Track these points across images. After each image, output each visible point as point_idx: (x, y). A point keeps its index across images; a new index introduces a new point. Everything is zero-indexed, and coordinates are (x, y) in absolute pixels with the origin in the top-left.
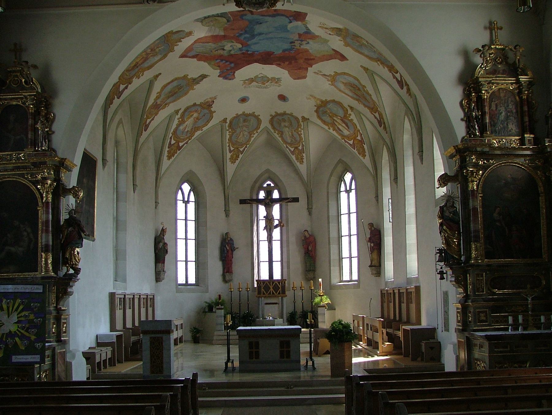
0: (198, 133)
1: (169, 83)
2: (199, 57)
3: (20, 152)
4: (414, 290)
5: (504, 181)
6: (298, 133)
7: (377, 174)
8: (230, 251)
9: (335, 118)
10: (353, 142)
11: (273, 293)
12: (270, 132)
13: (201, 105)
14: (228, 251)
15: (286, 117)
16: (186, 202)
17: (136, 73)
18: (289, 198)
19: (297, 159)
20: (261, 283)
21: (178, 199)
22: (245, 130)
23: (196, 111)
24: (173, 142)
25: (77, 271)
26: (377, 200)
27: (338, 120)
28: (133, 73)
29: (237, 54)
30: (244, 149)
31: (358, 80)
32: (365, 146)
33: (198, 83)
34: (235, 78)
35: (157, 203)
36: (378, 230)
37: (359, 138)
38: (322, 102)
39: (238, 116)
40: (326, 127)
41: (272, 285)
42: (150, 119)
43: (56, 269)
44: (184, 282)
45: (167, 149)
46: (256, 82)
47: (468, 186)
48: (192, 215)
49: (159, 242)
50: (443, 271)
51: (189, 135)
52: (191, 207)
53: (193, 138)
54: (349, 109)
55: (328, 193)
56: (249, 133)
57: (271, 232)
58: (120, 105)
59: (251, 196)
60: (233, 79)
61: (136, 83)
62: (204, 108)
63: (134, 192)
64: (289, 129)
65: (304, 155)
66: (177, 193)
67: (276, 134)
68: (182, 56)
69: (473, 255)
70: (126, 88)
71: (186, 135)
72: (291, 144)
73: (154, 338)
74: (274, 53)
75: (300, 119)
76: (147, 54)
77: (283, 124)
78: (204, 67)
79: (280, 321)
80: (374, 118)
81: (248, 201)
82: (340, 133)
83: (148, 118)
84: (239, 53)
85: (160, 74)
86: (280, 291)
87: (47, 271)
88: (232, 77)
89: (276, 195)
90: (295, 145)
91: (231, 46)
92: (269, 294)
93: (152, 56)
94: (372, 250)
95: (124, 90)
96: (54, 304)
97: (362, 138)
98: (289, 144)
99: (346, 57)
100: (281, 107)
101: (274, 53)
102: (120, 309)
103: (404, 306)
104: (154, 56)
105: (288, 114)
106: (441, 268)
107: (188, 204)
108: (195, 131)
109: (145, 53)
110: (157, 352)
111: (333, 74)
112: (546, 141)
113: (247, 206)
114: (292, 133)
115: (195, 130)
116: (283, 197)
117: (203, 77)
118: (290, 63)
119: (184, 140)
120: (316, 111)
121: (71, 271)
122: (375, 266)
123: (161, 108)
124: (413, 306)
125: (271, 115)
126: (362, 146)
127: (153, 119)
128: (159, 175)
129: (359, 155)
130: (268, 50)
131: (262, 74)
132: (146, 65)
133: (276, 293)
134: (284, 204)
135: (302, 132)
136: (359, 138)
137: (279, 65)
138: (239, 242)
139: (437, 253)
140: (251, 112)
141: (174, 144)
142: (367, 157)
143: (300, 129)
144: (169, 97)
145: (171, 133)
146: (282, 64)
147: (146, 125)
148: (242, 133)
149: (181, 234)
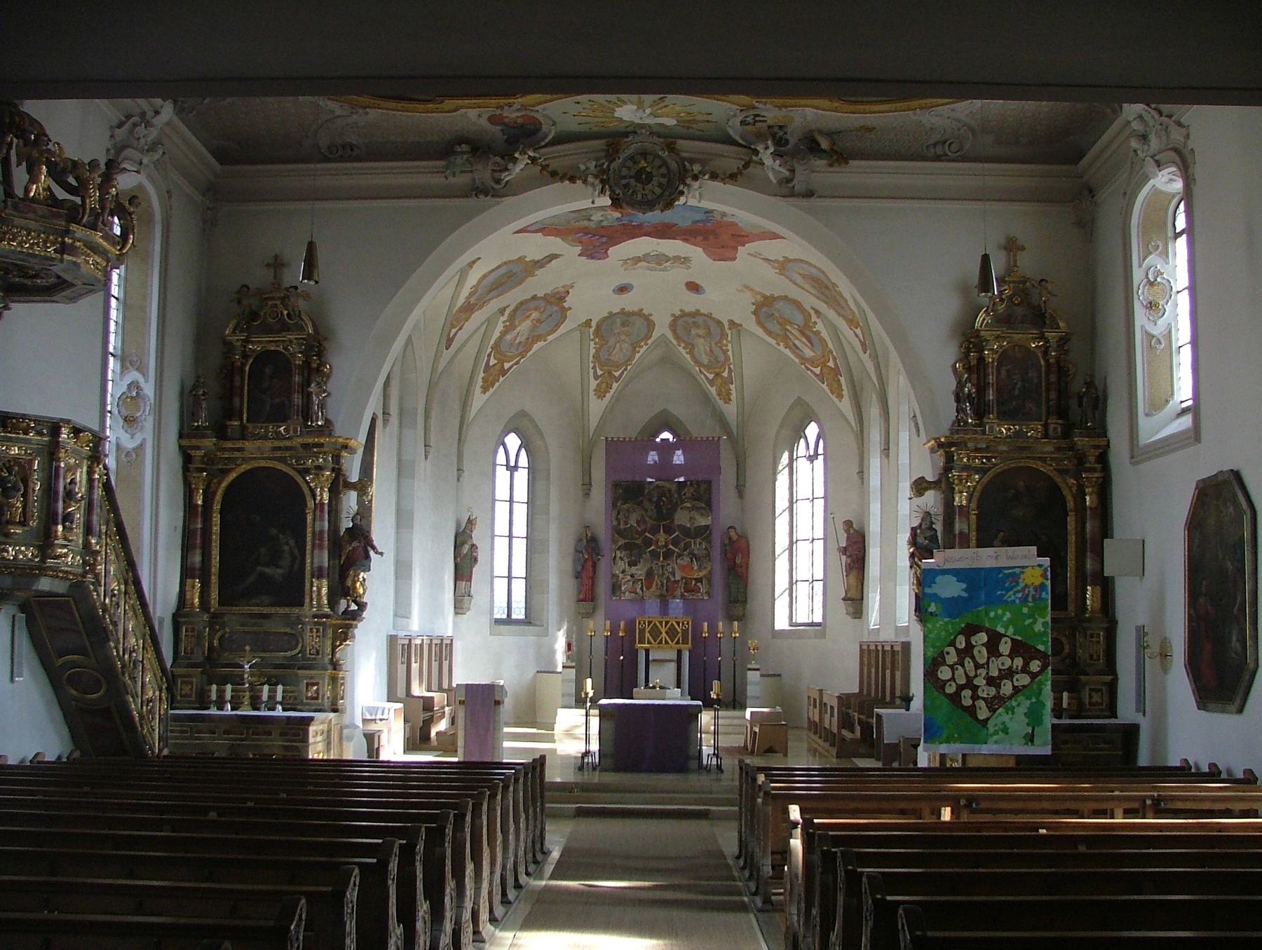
1: (493, 270)
3: (280, 424)
5: (1013, 491)
6: (721, 348)
7: (862, 431)
9: (788, 327)
11: (667, 642)
13: (545, 298)
15: (699, 320)
16: (513, 469)
20: (644, 623)
21: (497, 463)
22: (624, 340)
23: (536, 309)
24: (493, 362)
25: (362, 606)
26: (862, 479)
27: (793, 331)
30: (623, 373)
31: (823, 273)
32: (842, 379)
37: (831, 364)
38: (765, 297)
39: (611, 315)
40: (773, 342)
41: (666, 626)
43: (333, 603)
44: (505, 616)
45: (482, 375)
48: (521, 493)
49: (463, 543)
52: (522, 477)
54: (812, 312)
56: (632, 344)
60: (605, 258)
62: (551, 303)
63: (426, 458)
65: (732, 387)
66: (495, 452)
67: (681, 349)
71: (517, 350)
72: (708, 367)
75: (726, 326)
78: (555, 244)
82: (797, 353)
83: (453, 326)
85: (479, 258)
86: (679, 639)
87: (320, 605)
90: (715, 368)
94: (849, 569)
96: (329, 655)
97: (836, 365)
98: (704, 366)
100: (691, 302)
102: (402, 663)
103: (888, 672)
105: (705, 315)
107: (515, 473)
114: (710, 347)
115: (533, 341)
117: (553, 257)
121: (354, 607)
122: (852, 600)
125: (673, 315)
127: (460, 329)
128: (466, 420)
136: (831, 364)
137: (686, 240)
140: (636, 309)
142: (846, 400)
143: (725, 342)
148: (618, 345)
149: (501, 527)
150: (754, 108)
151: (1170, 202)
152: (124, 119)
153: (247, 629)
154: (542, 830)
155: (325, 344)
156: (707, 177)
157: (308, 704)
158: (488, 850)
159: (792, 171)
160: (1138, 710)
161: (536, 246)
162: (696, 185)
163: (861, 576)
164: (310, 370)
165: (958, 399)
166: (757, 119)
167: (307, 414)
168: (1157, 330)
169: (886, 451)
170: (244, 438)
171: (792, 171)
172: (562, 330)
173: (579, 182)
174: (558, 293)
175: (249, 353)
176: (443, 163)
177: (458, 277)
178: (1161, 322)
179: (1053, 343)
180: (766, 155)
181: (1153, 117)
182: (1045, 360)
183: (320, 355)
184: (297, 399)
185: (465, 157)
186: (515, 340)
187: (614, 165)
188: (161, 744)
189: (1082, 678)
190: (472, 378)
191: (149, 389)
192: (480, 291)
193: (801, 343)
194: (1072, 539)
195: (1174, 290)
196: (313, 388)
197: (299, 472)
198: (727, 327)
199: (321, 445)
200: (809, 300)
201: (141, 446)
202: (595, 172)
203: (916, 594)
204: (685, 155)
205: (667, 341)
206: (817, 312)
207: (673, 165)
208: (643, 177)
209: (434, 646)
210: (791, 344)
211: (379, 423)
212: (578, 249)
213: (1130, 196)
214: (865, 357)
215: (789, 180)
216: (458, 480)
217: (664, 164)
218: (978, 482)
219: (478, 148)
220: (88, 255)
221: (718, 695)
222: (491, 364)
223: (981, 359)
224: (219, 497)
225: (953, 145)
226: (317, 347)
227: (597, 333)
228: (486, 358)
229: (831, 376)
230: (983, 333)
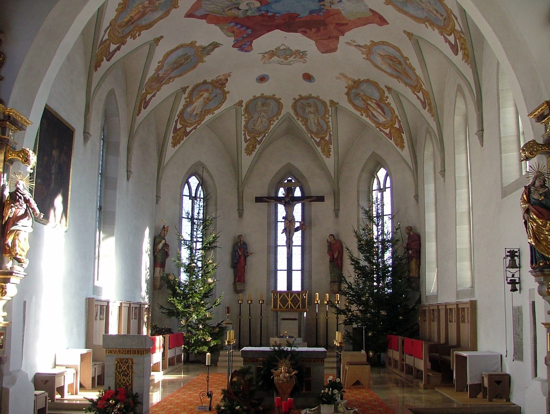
0: (208, 117)
1: (173, 51)
4: (468, 306)
6: (324, 120)
8: (243, 257)
9: (369, 102)
10: (390, 130)
12: (293, 120)
14: (240, 256)
15: (310, 101)
17: (130, 32)
18: (313, 196)
19: (323, 152)
22: (262, 116)
23: (207, 90)
24: (179, 126)
26: (417, 200)
27: (372, 105)
28: (127, 30)
29: (255, 16)
30: (262, 139)
31: (399, 51)
32: (404, 136)
33: (208, 54)
34: (253, 50)
35: (158, 197)
36: (418, 235)
37: (397, 126)
38: (355, 82)
39: (255, 99)
40: (358, 113)
41: (291, 297)
42: (151, 95)
45: (172, 135)
46: (278, 57)
50: (516, 280)
51: (199, 119)
53: (203, 122)
54: (385, 89)
55: (358, 191)
57: (291, 235)
58: (109, 70)
61: (131, 44)
64: (314, 115)
65: (332, 146)
67: (299, 122)
68: (189, 15)
70: (118, 48)
72: (316, 134)
74: (300, 15)
76: (144, 7)
77: (308, 110)
79: (299, 340)
80: (417, 99)
81: (265, 198)
83: (147, 93)
84: (257, 14)
85: (162, 37)
89: (298, 193)
91: (247, 4)
92: (286, 308)
93: (151, 11)
95: (115, 51)
99: (387, 20)
100: (306, 89)
101: (300, 15)
104: (153, 11)
106: (513, 276)
108: (205, 115)
109: (142, 5)
110: (124, 380)
111: (369, 44)
113: (264, 205)
116: (306, 195)
117: (215, 45)
119: (191, 124)
120: (347, 94)
123: (163, 82)
125: (294, 99)
126: (400, 136)
127: (154, 96)
129: (396, 147)
130: (292, 11)
131: (284, 45)
132: (143, 22)
133: (295, 306)
134: (306, 202)
135: (330, 119)
136: (397, 126)
137: (304, 33)
139: (507, 256)
140: (271, 95)
141: (180, 128)
143: (327, 116)
144: (173, 69)
145: (176, 116)
146: (308, 31)
147: (145, 102)
148: (259, 119)
163: (418, 263)
172: (224, 107)
174: (220, 80)
186: (193, 112)
192: (165, 67)
198: (328, 105)
203: (531, 246)
205: (291, 117)
210: (371, 114)
216: (157, 203)
221: (340, 343)
222: (178, 128)
227: (246, 111)
228: (174, 124)
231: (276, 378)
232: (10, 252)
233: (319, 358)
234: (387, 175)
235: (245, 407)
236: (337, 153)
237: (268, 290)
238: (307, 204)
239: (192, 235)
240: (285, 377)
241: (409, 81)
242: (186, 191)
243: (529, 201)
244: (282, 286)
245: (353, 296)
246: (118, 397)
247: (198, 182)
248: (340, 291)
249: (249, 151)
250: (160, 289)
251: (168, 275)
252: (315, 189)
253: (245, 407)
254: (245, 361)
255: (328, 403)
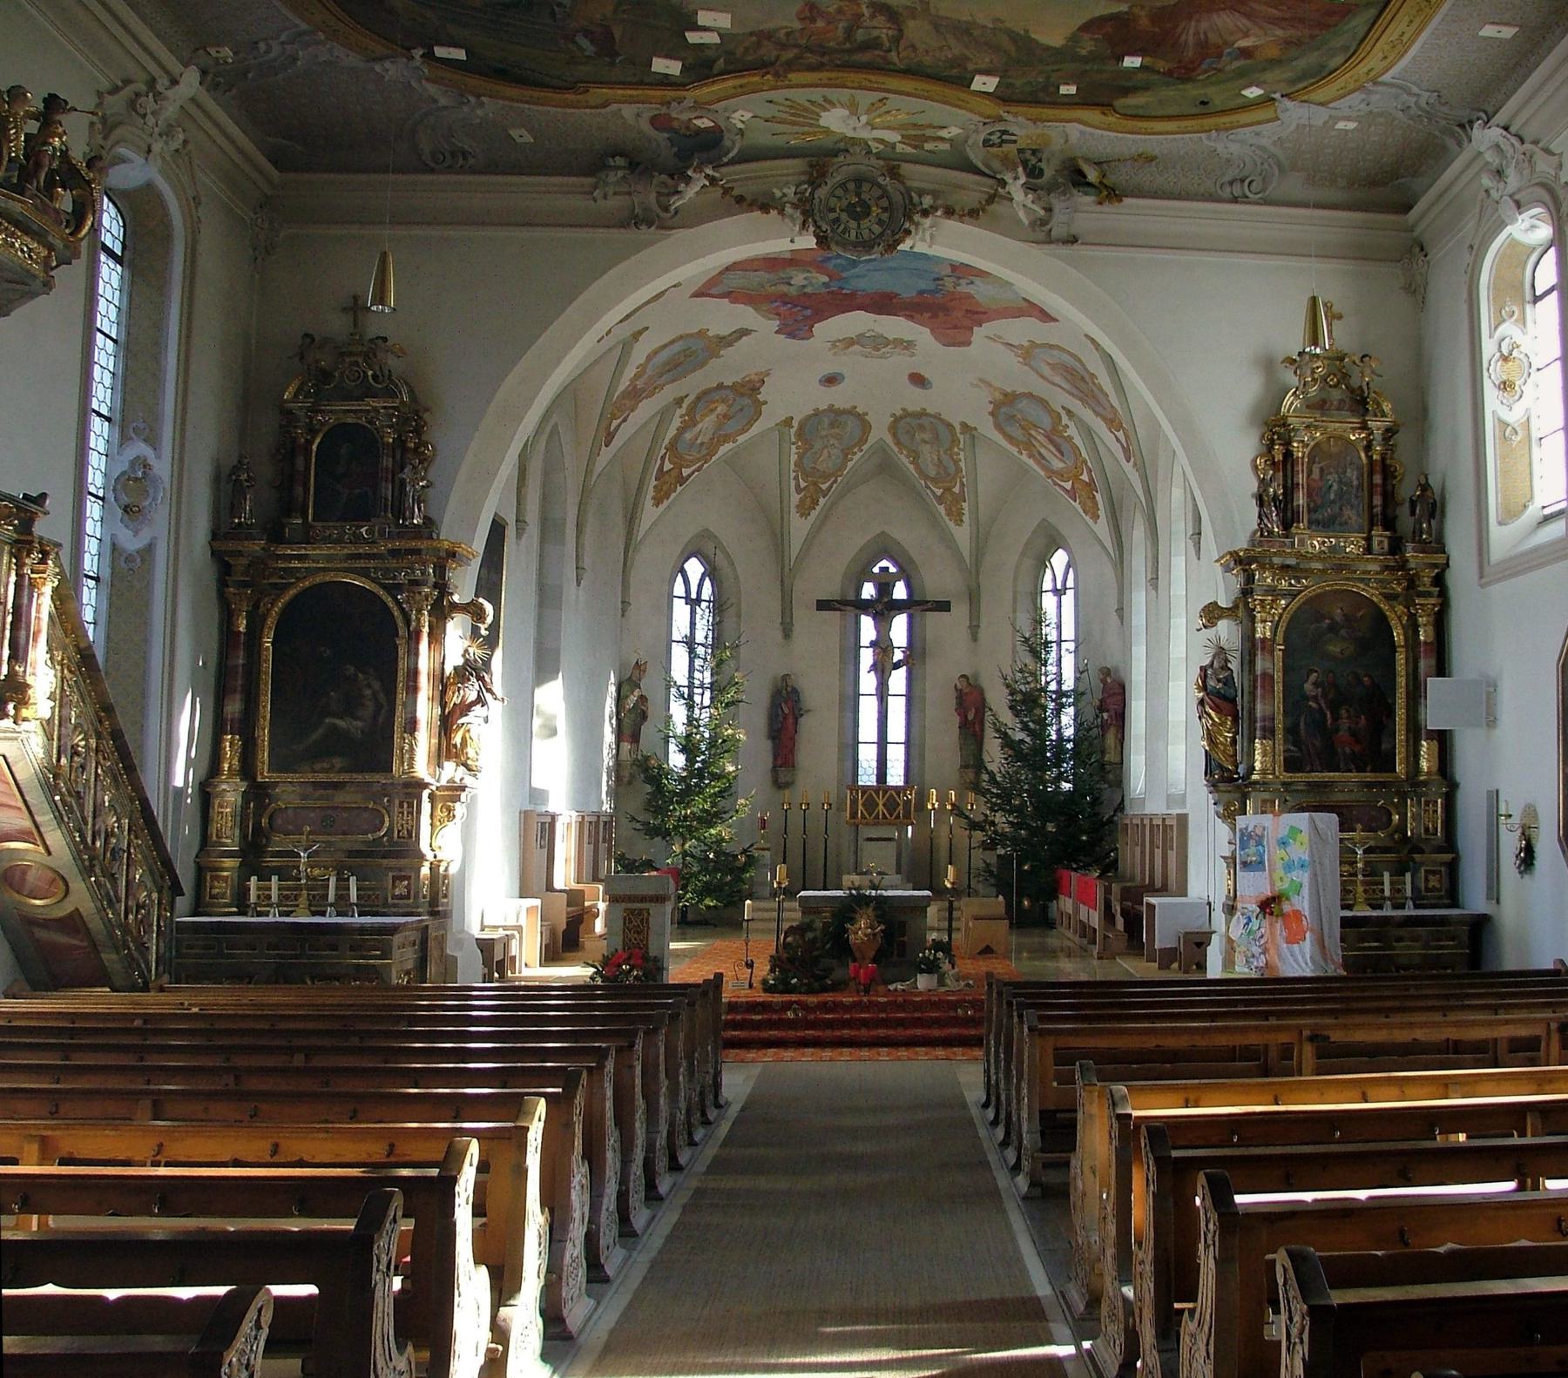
0: (725, 448)
1: (665, 346)
2: (732, 296)
6: (951, 457)
8: (791, 720)
9: (1033, 433)
13: (734, 387)
15: (925, 421)
23: (723, 401)
24: (668, 466)
26: (1121, 618)
30: (831, 486)
31: (1079, 360)
32: (1098, 496)
37: (1085, 477)
38: (1006, 395)
39: (817, 413)
40: (1014, 450)
45: (653, 483)
47: (1254, 630)
54: (1063, 414)
55: (1015, 593)
59: (769, 931)
62: (742, 395)
63: (579, 584)
65: (965, 505)
67: (902, 457)
69: (1258, 765)
72: (935, 481)
73: (632, 911)
78: (746, 316)
83: (614, 417)
84: (824, 290)
88: (809, 334)
89: (900, 592)
100: (915, 400)
103: (1158, 853)
105: (930, 415)
111: (1026, 344)
112: (1409, 549)
116: (916, 598)
117: (744, 332)
118: (935, 316)
119: (693, 462)
124: (1172, 856)
127: (624, 421)
130: (889, 290)
134: (916, 611)
136: (1085, 477)
137: (910, 317)
138: (817, 692)
140: (848, 406)
146: (918, 316)
148: (825, 451)
150: (1001, 119)
151: (1528, 257)
152: (120, 83)
153: (310, 803)
154: (717, 1075)
155: (426, 416)
156: (939, 213)
157: (394, 906)
158: (617, 1134)
159: (1049, 210)
160: (1489, 897)
161: (722, 317)
162: (927, 222)
164: (405, 449)
165: (1260, 499)
166: (1004, 137)
167: (400, 510)
168: (1513, 416)
169: (1154, 581)
170: (308, 541)
171: (1049, 210)
172: (756, 429)
173: (774, 213)
175: (317, 427)
176: (589, 180)
177: (619, 350)
178: (1516, 407)
179: (1378, 434)
180: (1016, 187)
181: (1512, 145)
182: (1367, 456)
183: (418, 431)
184: (387, 491)
185: (620, 173)
187: (822, 192)
188: (161, 968)
189: (1417, 857)
190: (640, 489)
191: (162, 467)
192: (649, 372)
193: (1048, 452)
194: (1401, 681)
195: (1534, 367)
196: (407, 474)
197: (384, 587)
199: (417, 552)
200: (1060, 398)
201: (150, 549)
202: (795, 201)
204: (915, 184)
206: (1069, 412)
207: (897, 198)
208: (859, 211)
209: (587, 825)
211: (510, 532)
212: (775, 324)
213: (1478, 252)
214: (1128, 467)
215: (1043, 223)
217: (885, 194)
218: (1284, 609)
219: (638, 163)
220: (13, 235)
221: (953, 883)
223: (1288, 455)
224: (271, 622)
225: (1254, 184)
226: (414, 420)
229: (1085, 492)
230: (1290, 420)
231: (852, 937)
232: (457, 756)
233: (919, 907)
234: (1068, 566)
235: (805, 981)
236: (976, 521)
237: (840, 781)
238: (918, 614)
239: (691, 677)
240: (866, 935)
241: (1099, 409)
242: (679, 588)
243: (1204, 688)
244: (867, 777)
245: (997, 796)
246: (632, 962)
247: (702, 570)
248: (976, 788)
249: (804, 510)
250: (630, 783)
251: (647, 759)
252: (934, 587)
253: (805, 981)
254: (803, 913)
255: (929, 971)
